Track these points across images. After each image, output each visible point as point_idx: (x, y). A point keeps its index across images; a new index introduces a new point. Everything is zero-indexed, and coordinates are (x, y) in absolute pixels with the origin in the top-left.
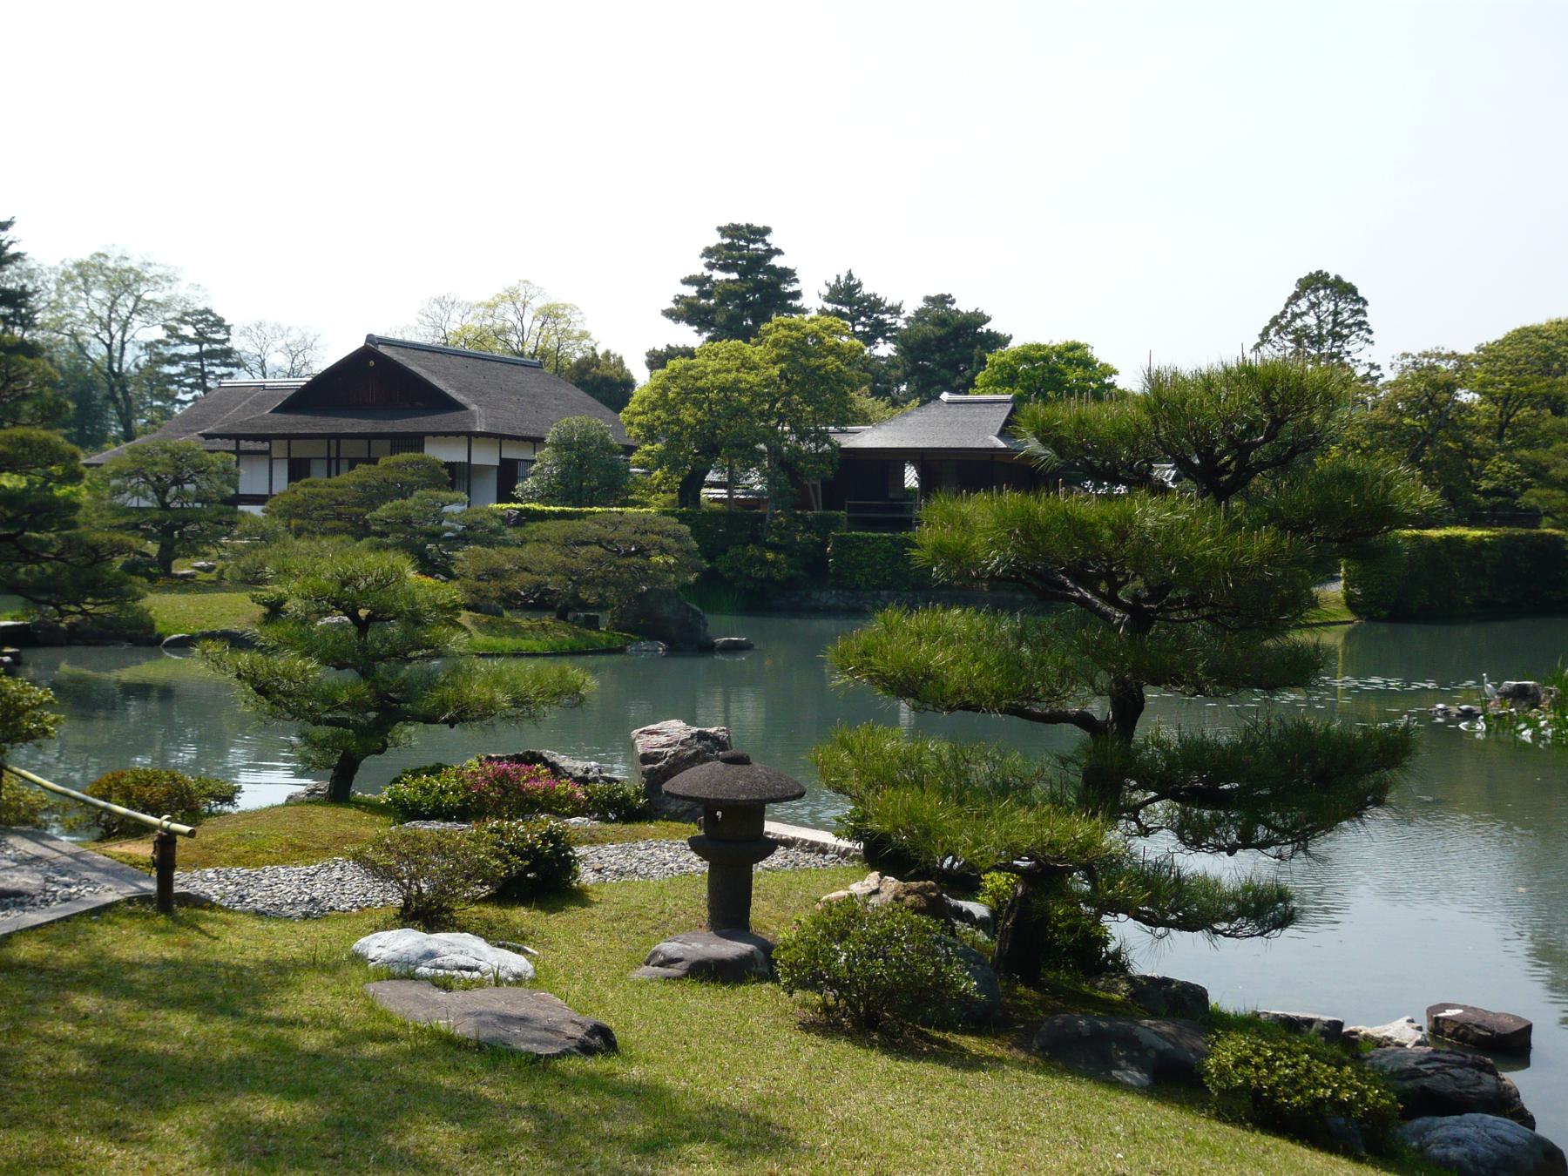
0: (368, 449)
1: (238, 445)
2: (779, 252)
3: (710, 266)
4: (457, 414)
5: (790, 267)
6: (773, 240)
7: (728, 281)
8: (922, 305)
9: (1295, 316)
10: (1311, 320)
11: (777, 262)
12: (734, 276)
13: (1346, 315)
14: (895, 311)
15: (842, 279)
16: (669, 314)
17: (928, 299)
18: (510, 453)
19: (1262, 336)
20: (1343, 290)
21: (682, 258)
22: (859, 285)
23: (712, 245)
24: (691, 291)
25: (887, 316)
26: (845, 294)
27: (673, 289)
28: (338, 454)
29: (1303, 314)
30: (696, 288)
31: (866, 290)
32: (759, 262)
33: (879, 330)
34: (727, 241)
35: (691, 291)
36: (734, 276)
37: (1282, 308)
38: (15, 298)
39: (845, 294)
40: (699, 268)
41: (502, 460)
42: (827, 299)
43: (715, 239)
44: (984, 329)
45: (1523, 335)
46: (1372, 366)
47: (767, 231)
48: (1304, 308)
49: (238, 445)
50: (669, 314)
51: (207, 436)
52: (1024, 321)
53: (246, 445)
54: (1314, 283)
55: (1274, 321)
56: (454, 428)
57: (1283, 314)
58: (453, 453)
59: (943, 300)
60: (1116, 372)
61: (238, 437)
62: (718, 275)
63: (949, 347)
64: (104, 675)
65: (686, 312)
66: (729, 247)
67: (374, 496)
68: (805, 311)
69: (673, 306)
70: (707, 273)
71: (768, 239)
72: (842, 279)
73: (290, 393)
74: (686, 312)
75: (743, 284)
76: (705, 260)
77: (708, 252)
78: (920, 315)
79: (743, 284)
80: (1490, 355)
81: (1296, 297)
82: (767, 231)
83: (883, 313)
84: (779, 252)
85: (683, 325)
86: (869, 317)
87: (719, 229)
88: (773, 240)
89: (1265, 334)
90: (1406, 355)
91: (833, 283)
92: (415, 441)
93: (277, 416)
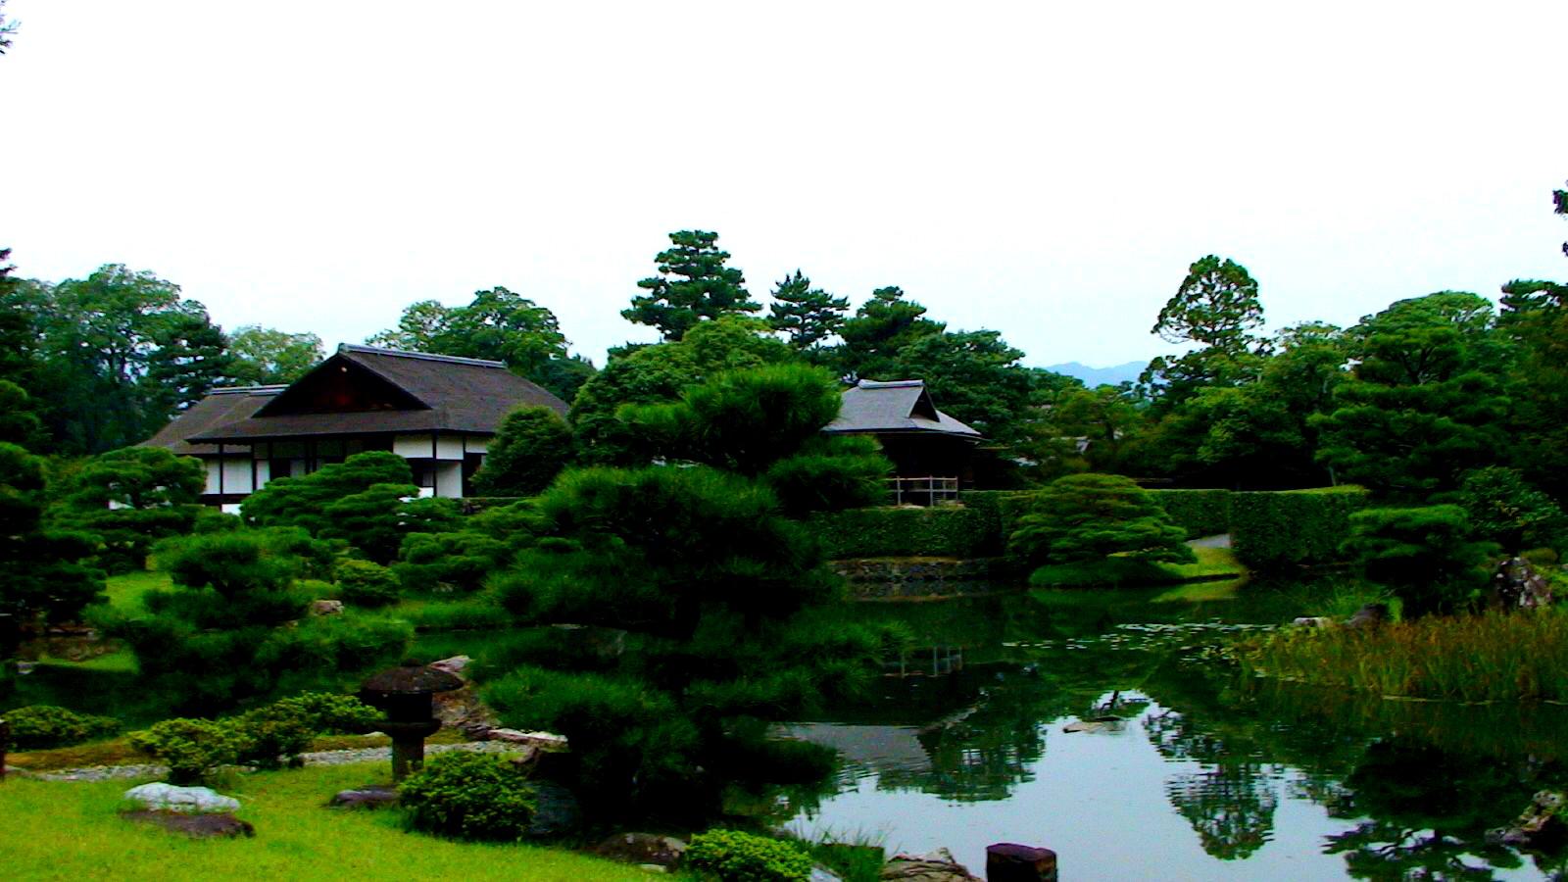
0: (340, 446)
1: (221, 449)
2: (727, 255)
3: (664, 270)
4: (423, 413)
5: (737, 268)
6: (721, 244)
7: (681, 283)
8: (873, 297)
9: (1191, 299)
10: (1205, 301)
11: (727, 265)
12: (686, 278)
13: (968, 345)
14: (842, 304)
15: (792, 279)
16: (626, 314)
17: (877, 292)
18: (472, 449)
19: (1160, 317)
20: (1236, 275)
21: (635, 261)
22: (807, 283)
23: (665, 251)
24: (647, 293)
25: (833, 309)
26: (794, 289)
27: (629, 292)
28: (311, 451)
29: (1200, 296)
30: (652, 290)
31: (812, 288)
32: (713, 264)
33: (828, 322)
34: (678, 247)
35: (647, 293)
36: (686, 278)
37: (1176, 292)
38: (15, 322)
39: (794, 289)
40: (653, 271)
41: (465, 454)
42: (778, 297)
43: (667, 245)
44: (920, 318)
45: (1402, 310)
46: (1264, 341)
47: (715, 236)
48: (1199, 290)
49: (221, 449)
50: (626, 314)
51: (193, 442)
52: (955, 311)
53: (228, 449)
54: (1205, 268)
55: (1172, 303)
56: (420, 427)
57: (1179, 296)
58: (423, 451)
59: (892, 292)
60: (1023, 355)
61: (221, 442)
62: (672, 277)
63: (889, 332)
64: (1439, 447)
65: (643, 313)
66: (682, 252)
67: (336, 488)
68: (759, 307)
69: (631, 307)
70: (661, 276)
71: (715, 243)
72: (792, 279)
73: (271, 398)
74: (643, 313)
75: (694, 283)
76: (659, 264)
77: (661, 258)
78: (869, 308)
79: (694, 283)
80: (1367, 327)
81: (1189, 281)
82: (715, 236)
83: (831, 306)
84: (727, 255)
85: (640, 325)
86: (818, 311)
87: (671, 235)
88: (721, 244)
89: (1162, 316)
90: (1287, 330)
91: (783, 281)
92: (386, 440)
93: (260, 420)
